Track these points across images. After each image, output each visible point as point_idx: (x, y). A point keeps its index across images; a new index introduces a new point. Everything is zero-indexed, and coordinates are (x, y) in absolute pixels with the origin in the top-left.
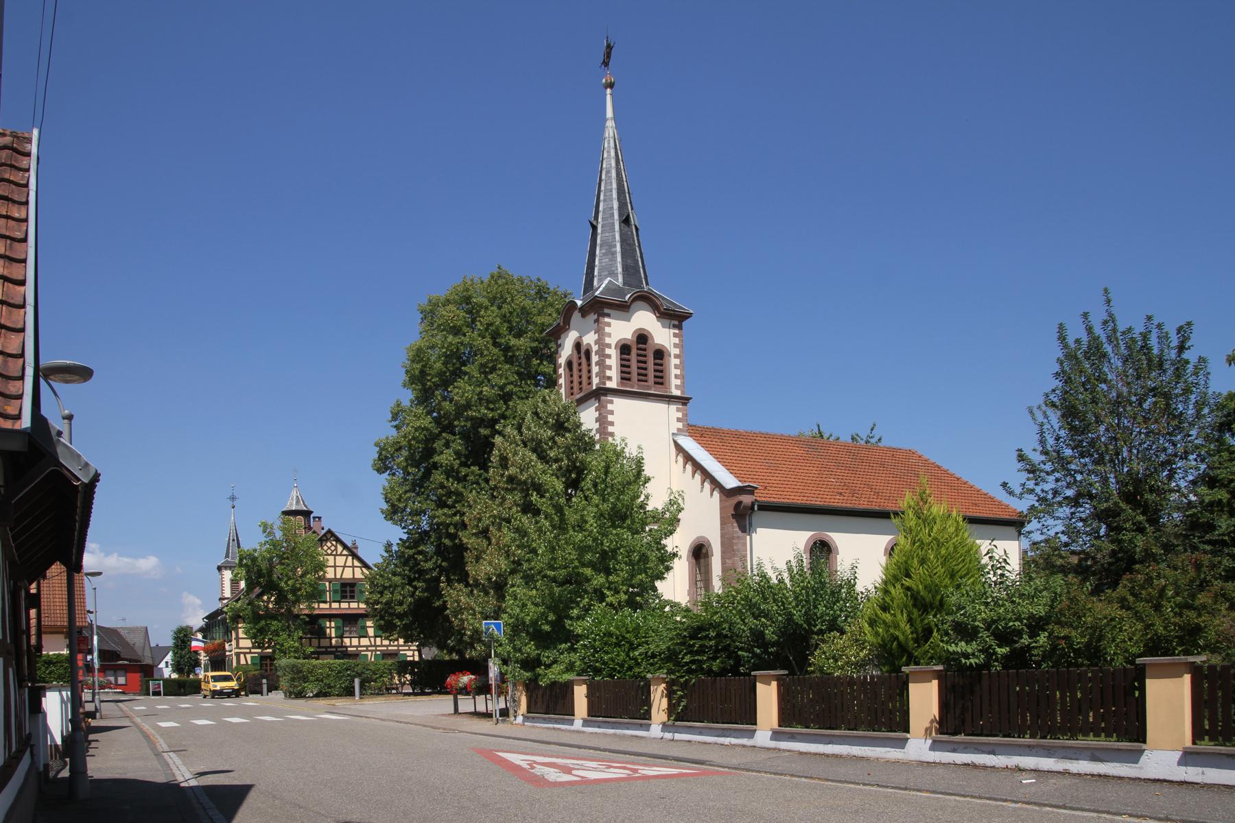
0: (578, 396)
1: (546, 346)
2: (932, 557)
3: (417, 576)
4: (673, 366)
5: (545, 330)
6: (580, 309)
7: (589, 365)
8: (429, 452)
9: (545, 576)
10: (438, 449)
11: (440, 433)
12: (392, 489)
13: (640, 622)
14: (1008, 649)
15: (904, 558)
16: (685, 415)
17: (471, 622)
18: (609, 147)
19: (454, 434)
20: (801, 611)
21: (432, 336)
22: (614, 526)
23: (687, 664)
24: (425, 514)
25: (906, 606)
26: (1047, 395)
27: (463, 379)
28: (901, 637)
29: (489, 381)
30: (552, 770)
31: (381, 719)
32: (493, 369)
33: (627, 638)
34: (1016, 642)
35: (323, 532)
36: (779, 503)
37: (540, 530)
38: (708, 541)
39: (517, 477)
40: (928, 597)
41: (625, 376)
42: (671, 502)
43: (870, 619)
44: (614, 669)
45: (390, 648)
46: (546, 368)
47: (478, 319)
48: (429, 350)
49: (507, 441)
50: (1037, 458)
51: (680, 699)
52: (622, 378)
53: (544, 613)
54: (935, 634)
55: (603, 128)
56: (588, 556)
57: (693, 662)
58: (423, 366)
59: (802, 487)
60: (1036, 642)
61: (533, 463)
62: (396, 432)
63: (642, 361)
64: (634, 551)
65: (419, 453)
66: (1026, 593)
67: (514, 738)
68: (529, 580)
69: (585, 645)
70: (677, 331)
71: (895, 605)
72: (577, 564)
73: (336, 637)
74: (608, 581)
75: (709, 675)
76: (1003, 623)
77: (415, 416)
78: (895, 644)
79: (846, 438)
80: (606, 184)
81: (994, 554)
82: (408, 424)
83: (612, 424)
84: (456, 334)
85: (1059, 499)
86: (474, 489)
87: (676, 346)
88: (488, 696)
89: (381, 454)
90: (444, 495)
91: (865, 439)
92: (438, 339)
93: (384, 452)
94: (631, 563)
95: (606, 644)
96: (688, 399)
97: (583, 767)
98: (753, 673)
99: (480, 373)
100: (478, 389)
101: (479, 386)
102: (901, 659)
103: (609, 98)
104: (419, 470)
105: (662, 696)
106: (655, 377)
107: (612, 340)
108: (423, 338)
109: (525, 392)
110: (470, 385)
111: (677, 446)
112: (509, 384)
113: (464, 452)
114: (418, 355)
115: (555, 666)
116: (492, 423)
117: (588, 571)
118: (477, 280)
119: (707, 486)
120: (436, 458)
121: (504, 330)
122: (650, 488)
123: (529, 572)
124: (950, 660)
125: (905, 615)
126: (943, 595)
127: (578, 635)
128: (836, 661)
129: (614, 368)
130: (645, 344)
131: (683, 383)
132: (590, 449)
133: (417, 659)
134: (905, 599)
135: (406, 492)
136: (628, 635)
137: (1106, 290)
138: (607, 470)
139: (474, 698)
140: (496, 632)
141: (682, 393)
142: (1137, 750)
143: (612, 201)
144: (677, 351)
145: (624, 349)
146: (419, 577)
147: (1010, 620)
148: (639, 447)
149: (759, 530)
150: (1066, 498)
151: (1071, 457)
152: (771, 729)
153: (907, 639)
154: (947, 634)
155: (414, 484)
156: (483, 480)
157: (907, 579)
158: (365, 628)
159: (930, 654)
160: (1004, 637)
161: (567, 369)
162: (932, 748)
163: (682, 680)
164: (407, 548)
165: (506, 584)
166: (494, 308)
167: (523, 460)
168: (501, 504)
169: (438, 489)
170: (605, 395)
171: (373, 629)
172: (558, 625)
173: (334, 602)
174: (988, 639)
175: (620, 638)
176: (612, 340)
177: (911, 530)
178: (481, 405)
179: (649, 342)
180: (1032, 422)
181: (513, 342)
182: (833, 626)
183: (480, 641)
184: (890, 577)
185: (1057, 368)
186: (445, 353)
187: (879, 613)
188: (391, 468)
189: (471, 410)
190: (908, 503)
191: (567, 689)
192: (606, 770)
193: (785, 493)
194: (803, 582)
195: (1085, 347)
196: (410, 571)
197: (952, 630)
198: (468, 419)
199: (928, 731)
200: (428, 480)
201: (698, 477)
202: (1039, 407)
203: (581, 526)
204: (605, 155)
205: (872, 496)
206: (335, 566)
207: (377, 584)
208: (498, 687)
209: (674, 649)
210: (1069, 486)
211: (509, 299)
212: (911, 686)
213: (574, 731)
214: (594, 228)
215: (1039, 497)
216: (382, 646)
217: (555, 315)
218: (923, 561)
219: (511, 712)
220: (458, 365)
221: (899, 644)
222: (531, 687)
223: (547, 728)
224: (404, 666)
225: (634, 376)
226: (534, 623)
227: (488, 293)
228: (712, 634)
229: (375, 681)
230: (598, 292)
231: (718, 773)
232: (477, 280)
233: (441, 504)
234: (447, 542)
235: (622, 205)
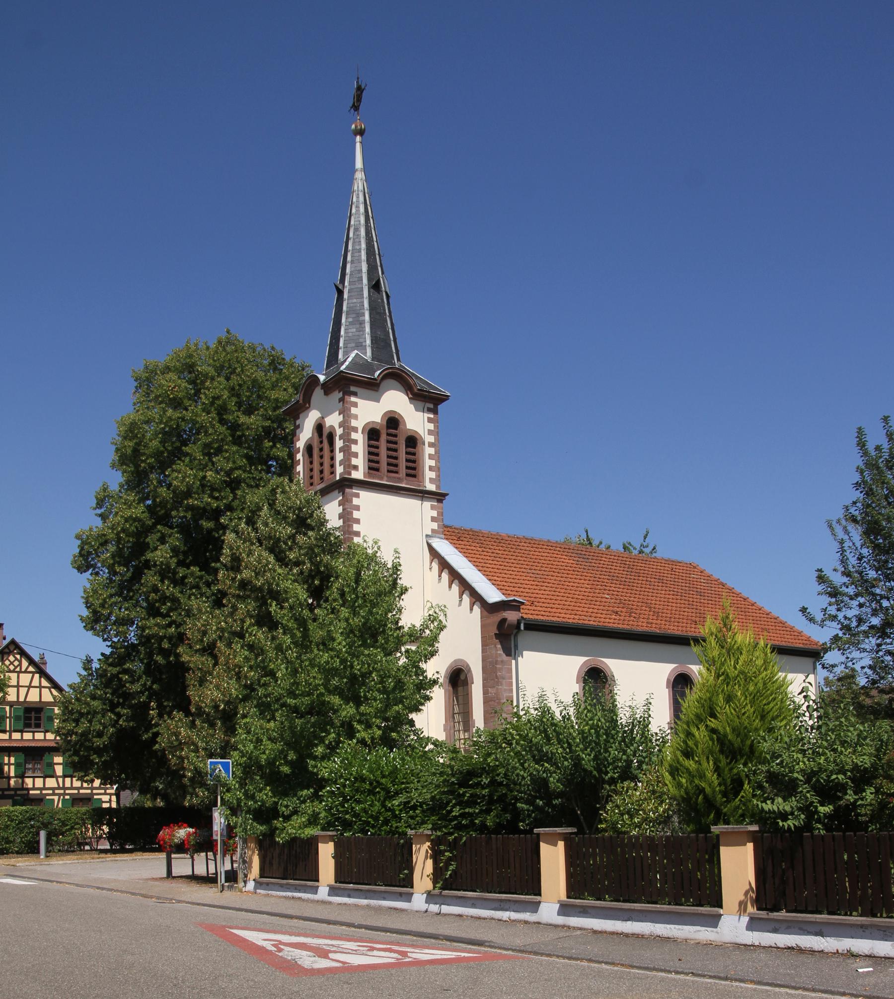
0: (319, 487)
1: (280, 426)
2: (739, 694)
4: (427, 456)
5: (280, 407)
7: (332, 451)
8: (140, 548)
9: (284, 705)
11: (155, 525)
12: (95, 591)
13: (398, 763)
14: (831, 807)
15: (708, 695)
16: (441, 514)
17: (193, 761)
18: (358, 201)
19: (171, 527)
20: (590, 755)
21: (148, 408)
22: (365, 645)
23: (455, 817)
24: (133, 623)
25: (711, 752)
26: (847, 508)
27: (183, 461)
28: (708, 790)
29: (213, 464)
30: (305, 953)
31: (77, 885)
32: (219, 451)
33: (382, 784)
34: (840, 799)
35: (5, 643)
36: (547, 622)
37: (279, 648)
38: (468, 665)
39: (252, 582)
40: (737, 742)
41: (373, 466)
42: (432, 619)
43: (670, 766)
44: (368, 823)
45: (82, 791)
46: (280, 451)
47: (202, 391)
48: (144, 426)
49: (240, 538)
50: (838, 579)
51: (448, 863)
52: (370, 468)
53: (283, 750)
54: (746, 786)
55: (351, 180)
56: (335, 682)
57: (463, 815)
58: (136, 443)
59: (573, 604)
60: (862, 799)
61: (270, 566)
62: (101, 522)
64: (389, 677)
65: (128, 548)
66: (849, 740)
67: (247, 911)
68: (265, 709)
69: (333, 792)
70: (432, 416)
71: (700, 750)
72: (323, 691)
73: (16, 777)
74: (358, 712)
75: (482, 833)
76: (824, 776)
77: (125, 504)
78: (701, 797)
79: (617, 547)
80: (354, 243)
81: (809, 693)
82: (117, 513)
83: (358, 521)
84: (175, 408)
85: (864, 627)
86: (193, 594)
87: (430, 432)
88: (210, 854)
89: (82, 549)
90: (156, 601)
91: (638, 548)
92: (155, 413)
93: (86, 547)
94: (384, 691)
95: (357, 791)
97: (341, 950)
98: (536, 830)
99: (204, 454)
102: (708, 816)
103: (358, 146)
104: (128, 570)
105: (426, 858)
106: (407, 468)
107: (359, 424)
108: (138, 411)
109: (254, 478)
110: (192, 469)
111: (431, 549)
112: (237, 469)
113: (182, 549)
114: (132, 431)
115: (295, 817)
116: (217, 514)
117: (336, 700)
118: (202, 345)
119: (466, 598)
120: (149, 555)
121: (232, 405)
122: (406, 602)
123: (264, 699)
124: (767, 821)
125: (711, 763)
126: (753, 741)
127: (323, 779)
128: (631, 817)
129: (361, 455)
130: (396, 429)
131: (438, 476)
132: (336, 551)
133: (114, 805)
134: (711, 743)
135: (111, 596)
136: (383, 781)
138: (358, 578)
139: (192, 858)
141: (438, 487)
142: (536, 902)
144: (431, 439)
145: (373, 434)
146: (124, 701)
147: (832, 772)
148: (396, 552)
149: (526, 653)
150: (872, 627)
151: (875, 579)
152: (559, 901)
153: (714, 791)
154: (760, 787)
155: (121, 587)
156: (204, 583)
157: (712, 720)
158: (51, 765)
159: (740, 811)
160: (828, 792)
161: (307, 456)
162: (751, 927)
163: (451, 838)
164: (111, 665)
165: (236, 714)
166: (222, 379)
167: (259, 562)
168: (232, 614)
169: (150, 592)
170: (351, 487)
171: (61, 767)
172: (299, 766)
173: (15, 731)
174: (808, 795)
175: (375, 784)
176: (359, 424)
177: (714, 661)
178: (203, 492)
179: (401, 426)
180: (832, 537)
181: (243, 419)
182: (627, 774)
183: (203, 785)
184: (693, 717)
185: (857, 478)
186: (163, 428)
187: (681, 759)
188: (94, 566)
189: (192, 497)
190: (710, 629)
191: (309, 848)
192: (369, 953)
193: (554, 610)
194: (591, 719)
195: (886, 456)
196: (112, 694)
197: (767, 782)
199: (742, 906)
200: (139, 581)
201: (455, 588)
202: (838, 522)
203: (325, 644)
204: (354, 211)
205: (651, 617)
206: (18, 686)
207: (72, 709)
208: (224, 843)
209: (441, 799)
210: (875, 613)
211: (239, 369)
212: (723, 850)
213: (318, 901)
214: (340, 292)
215: (842, 624)
216: (72, 788)
217: (290, 390)
218: (729, 699)
219: (240, 876)
220: (178, 444)
221: (706, 797)
222: (266, 844)
223: (285, 897)
224: (100, 815)
225: (384, 466)
226: (271, 763)
227: (214, 361)
228: (484, 780)
229: (63, 834)
231: (500, 957)
232: (202, 345)
233: (153, 611)
234: (159, 659)
235: (372, 269)
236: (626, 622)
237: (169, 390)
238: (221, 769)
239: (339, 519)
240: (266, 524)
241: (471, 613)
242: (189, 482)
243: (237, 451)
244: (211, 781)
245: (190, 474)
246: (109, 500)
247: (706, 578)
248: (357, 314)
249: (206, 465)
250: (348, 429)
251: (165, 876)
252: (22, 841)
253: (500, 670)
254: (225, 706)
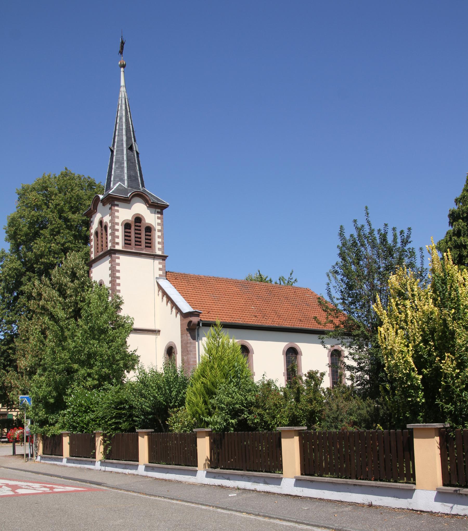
3: (9, 363)
4: (157, 237)
6: (102, 200)
7: (107, 235)
8: (19, 284)
10: (24, 282)
16: (164, 266)
19: (34, 273)
32: (58, 233)
34: (240, 416)
38: (175, 345)
41: (127, 242)
44: (83, 427)
52: (125, 244)
55: (119, 91)
63: (138, 234)
70: (159, 216)
83: (119, 271)
87: (159, 224)
91: (287, 280)
95: (79, 411)
96: (166, 257)
99: (51, 235)
100: (48, 245)
101: (49, 243)
105: (101, 444)
106: (146, 243)
112: (68, 242)
114: (13, 222)
118: (52, 176)
121: (66, 208)
130: (140, 223)
131: (163, 247)
137: (366, 208)
140: (27, 403)
141: (163, 252)
143: (123, 136)
144: (159, 228)
145: (127, 226)
160: (235, 413)
161: (96, 237)
170: (115, 254)
179: (143, 222)
196: (4, 360)
198: (42, 263)
204: (119, 108)
214: (112, 151)
223: (51, 464)
225: (133, 242)
226: (45, 398)
230: (111, 191)
232: (52, 176)
235: (128, 139)
236: (260, 321)
237: (33, 201)
238: (26, 400)
239: (110, 283)
240: (55, 277)
241: (176, 318)
242: (42, 250)
243: (69, 233)
244: (21, 406)
245: (42, 245)
246: (5, 258)
247: (314, 296)
248: (120, 163)
249: (52, 240)
250: (114, 224)
251: (12, 454)
253: (190, 347)
254: (30, 369)
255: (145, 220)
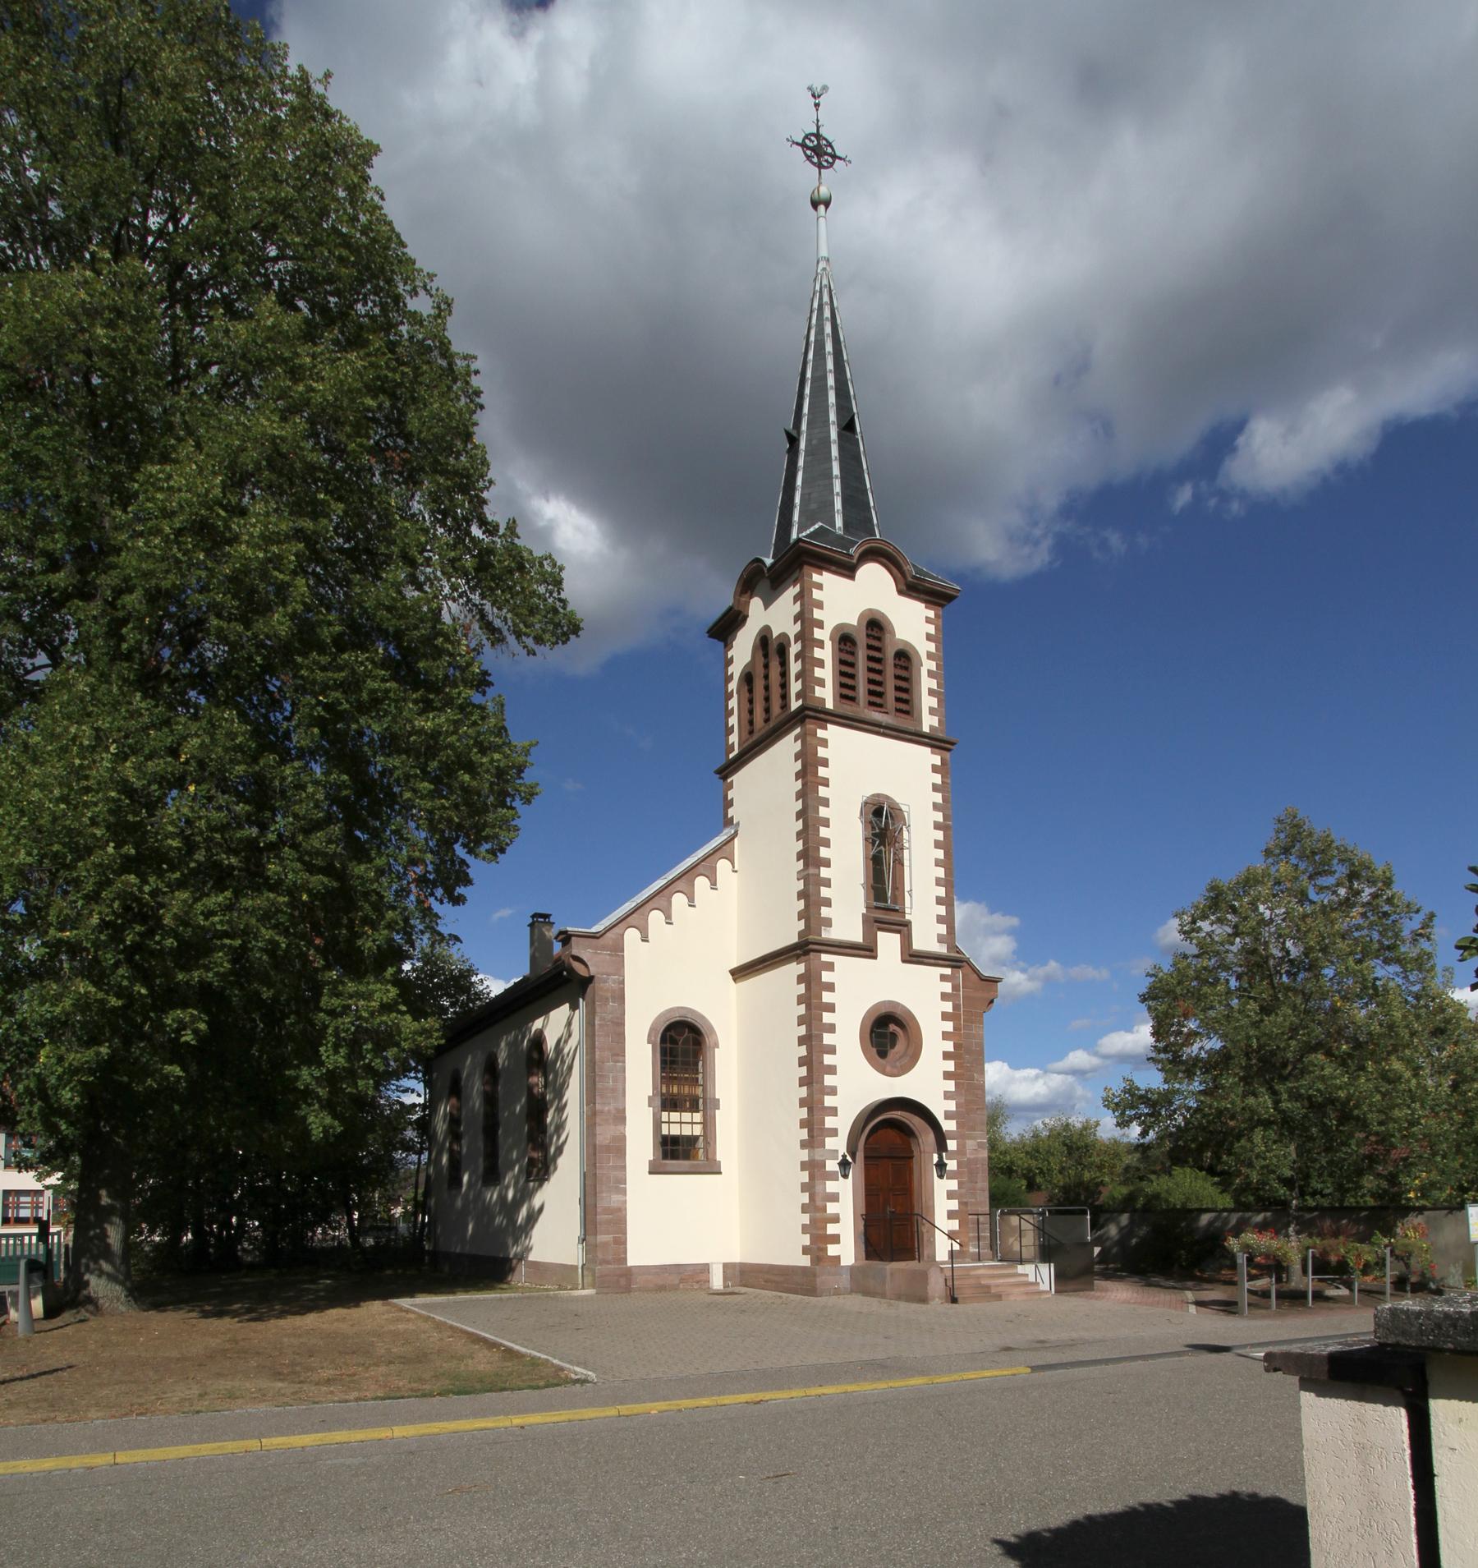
41: (846, 691)
129: (828, 644)
179: (888, 636)
239: (798, 860)
252: (88, 342)
255: (893, 633)
